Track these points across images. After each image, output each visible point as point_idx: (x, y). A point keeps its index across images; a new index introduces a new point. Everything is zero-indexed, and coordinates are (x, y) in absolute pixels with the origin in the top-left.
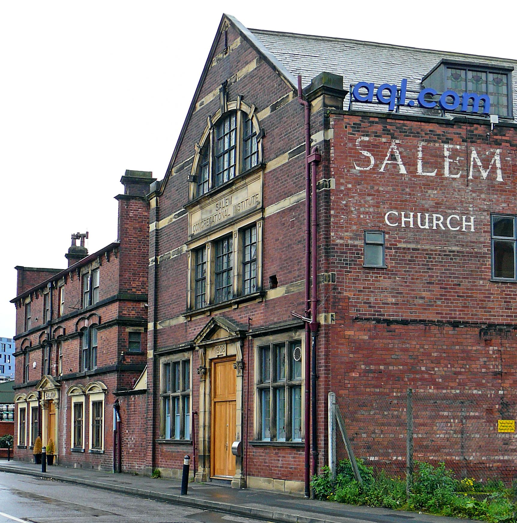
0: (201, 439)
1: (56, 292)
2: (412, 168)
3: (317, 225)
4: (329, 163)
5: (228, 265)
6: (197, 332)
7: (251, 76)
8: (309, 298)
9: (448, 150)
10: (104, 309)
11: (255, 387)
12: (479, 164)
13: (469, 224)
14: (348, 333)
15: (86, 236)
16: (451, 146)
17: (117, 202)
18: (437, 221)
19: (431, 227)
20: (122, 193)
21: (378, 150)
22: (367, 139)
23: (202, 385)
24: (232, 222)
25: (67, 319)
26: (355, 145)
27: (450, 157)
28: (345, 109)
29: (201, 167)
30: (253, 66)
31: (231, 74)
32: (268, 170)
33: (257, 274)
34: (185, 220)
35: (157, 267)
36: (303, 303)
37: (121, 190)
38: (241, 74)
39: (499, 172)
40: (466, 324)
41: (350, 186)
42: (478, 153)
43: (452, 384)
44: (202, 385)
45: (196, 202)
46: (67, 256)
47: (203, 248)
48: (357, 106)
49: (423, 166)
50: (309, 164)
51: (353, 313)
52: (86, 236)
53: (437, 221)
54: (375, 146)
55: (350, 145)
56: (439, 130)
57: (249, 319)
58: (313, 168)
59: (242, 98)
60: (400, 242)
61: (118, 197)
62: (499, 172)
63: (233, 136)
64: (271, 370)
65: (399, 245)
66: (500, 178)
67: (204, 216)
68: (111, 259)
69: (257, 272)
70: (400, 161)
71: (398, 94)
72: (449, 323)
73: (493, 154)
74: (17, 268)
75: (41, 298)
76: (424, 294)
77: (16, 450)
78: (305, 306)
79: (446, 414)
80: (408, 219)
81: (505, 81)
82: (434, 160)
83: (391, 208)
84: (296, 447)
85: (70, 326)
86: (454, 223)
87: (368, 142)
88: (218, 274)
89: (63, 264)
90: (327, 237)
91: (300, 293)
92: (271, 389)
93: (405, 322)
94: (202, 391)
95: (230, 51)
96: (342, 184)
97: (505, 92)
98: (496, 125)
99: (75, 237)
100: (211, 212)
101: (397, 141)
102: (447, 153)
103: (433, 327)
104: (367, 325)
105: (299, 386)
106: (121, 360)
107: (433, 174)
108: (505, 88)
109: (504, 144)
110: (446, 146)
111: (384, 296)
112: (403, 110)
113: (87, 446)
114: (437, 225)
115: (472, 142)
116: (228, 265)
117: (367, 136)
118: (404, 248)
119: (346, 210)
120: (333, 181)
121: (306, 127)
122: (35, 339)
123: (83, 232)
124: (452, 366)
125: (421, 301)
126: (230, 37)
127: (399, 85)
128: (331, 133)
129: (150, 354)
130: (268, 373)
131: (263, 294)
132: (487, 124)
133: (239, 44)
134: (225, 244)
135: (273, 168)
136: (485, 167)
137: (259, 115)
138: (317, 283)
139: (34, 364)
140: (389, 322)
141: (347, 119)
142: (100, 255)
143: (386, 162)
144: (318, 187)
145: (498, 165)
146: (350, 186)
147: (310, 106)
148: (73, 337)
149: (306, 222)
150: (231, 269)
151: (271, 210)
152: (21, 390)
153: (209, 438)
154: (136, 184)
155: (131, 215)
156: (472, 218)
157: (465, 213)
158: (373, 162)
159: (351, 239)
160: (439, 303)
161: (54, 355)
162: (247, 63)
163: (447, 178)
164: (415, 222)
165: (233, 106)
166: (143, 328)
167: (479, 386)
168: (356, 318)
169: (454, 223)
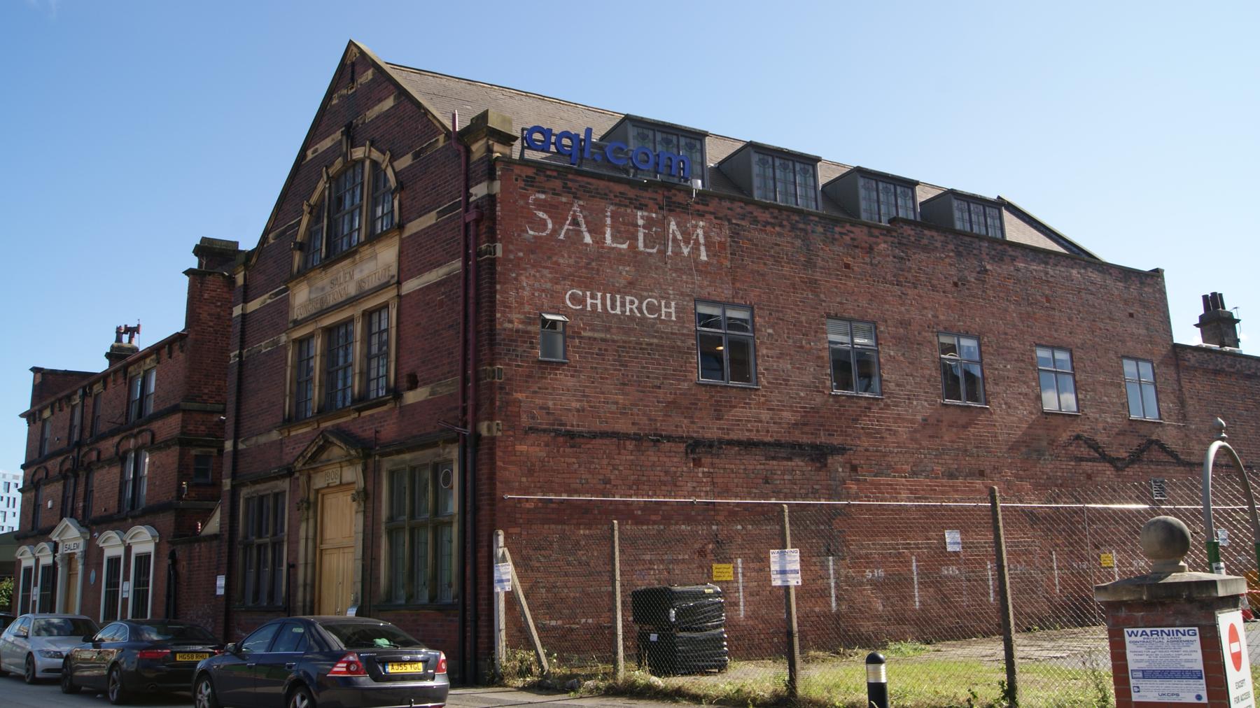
0: (300, 604)
1: (90, 401)
2: (598, 237)
3: (478, 304)
4: (495, 224)
5: (346, 361)
6: (297, 452)
7: (386, 115)
8: (464, 401)
9: (642, 217)
10: (160, 423)
11: (383, 527)
12: (679, 237)
13: (669, 311)
16: (646, 214)
17: (186, 279)
18: (630, 305)
19: (623, 312)
20: (195, 266)
21: (557, 213)
22: (542, 196)
23: (303, 526)
24: (351, 301)
25: (104, 437)
26: (528, 203)
27: (644, 227)
30: (389, 103)
31: (358, 114)
32: (407, 233)
33: (388, 371)
35: (241, 364)
36: (456, 408)
37: (194, 263)
38: (372, 114)
39: (703, 248)
40: (669, 438)
41: (521, 254)
42: (678, 224)
43: (653, 518)
45: (303, 274)
46: (108, 355)
48: (531, 155)
49: (612, 235)
50: (467, 226)
51: (525, 420)
53: (630, 305)
54: (552, 206)
55: (521, 202)
56: (631, 193)
57: (377, 432)
58: (472, 228)
59: (372, 144)
60: (585, 329)
62: (703, 248)
63: (358, 192)
64: (407, 502)
67: (313, 296)
68: (174, 355)
69: (388, 371)
70: (584, 228)
73: (696, 226)
74: (35, 370)
78: (459, 413)
80: (595, 301)
81: (698, 146)
83: (572, 287)
84: (444, 609)
85: (108, 446)
87: (545, 200)
88: (329, 373)
89: (100, 365)
90: (492, 320)
91: (451, 395)
92: (407, 528)
94: (302, 533)
95: (357, 85)
96: (511, 251)
97: (699, 160)
98: (699, 194)
100: (323, 289)
101: (581, 203)
102: (640, 222)
104: (546, 438)
108: (698, 155)
109: (707, 216)
110: (639, 213)
114: (631, 310)
115: (670, 210)
116: (346, 361)
117: (543, 192)
118: (590, 338)
120: (499, 246)
121: (462, 177)
122: (54, 465)
123: (132, 324)
124: (655, 495)
126: (358, 68)
128: (497, 187)
129: (227, 483)
132: (689, 191)
133: (370, 77)
134: (342, 331)
135: (415, 230)
136: (687, 242)
137: (395, 164)
140: (571, 435)
142: (157, 349)
143: (566, 227)
144: (479, 254)
145: (702, 240)
146: (521, 254)
147: (468, 151)
148: (110, 462)
149: (461, 300)
150: (351, 365)
153: (312, 602)
154: (214, 257)
155: (206, 296)
156: (673, 304)
158: (550, 226)
161: (81, 490)
162: (380, 100)
164: (604, 304)
165: (358, 153)
168: (530, 429)
169: (651, 309)
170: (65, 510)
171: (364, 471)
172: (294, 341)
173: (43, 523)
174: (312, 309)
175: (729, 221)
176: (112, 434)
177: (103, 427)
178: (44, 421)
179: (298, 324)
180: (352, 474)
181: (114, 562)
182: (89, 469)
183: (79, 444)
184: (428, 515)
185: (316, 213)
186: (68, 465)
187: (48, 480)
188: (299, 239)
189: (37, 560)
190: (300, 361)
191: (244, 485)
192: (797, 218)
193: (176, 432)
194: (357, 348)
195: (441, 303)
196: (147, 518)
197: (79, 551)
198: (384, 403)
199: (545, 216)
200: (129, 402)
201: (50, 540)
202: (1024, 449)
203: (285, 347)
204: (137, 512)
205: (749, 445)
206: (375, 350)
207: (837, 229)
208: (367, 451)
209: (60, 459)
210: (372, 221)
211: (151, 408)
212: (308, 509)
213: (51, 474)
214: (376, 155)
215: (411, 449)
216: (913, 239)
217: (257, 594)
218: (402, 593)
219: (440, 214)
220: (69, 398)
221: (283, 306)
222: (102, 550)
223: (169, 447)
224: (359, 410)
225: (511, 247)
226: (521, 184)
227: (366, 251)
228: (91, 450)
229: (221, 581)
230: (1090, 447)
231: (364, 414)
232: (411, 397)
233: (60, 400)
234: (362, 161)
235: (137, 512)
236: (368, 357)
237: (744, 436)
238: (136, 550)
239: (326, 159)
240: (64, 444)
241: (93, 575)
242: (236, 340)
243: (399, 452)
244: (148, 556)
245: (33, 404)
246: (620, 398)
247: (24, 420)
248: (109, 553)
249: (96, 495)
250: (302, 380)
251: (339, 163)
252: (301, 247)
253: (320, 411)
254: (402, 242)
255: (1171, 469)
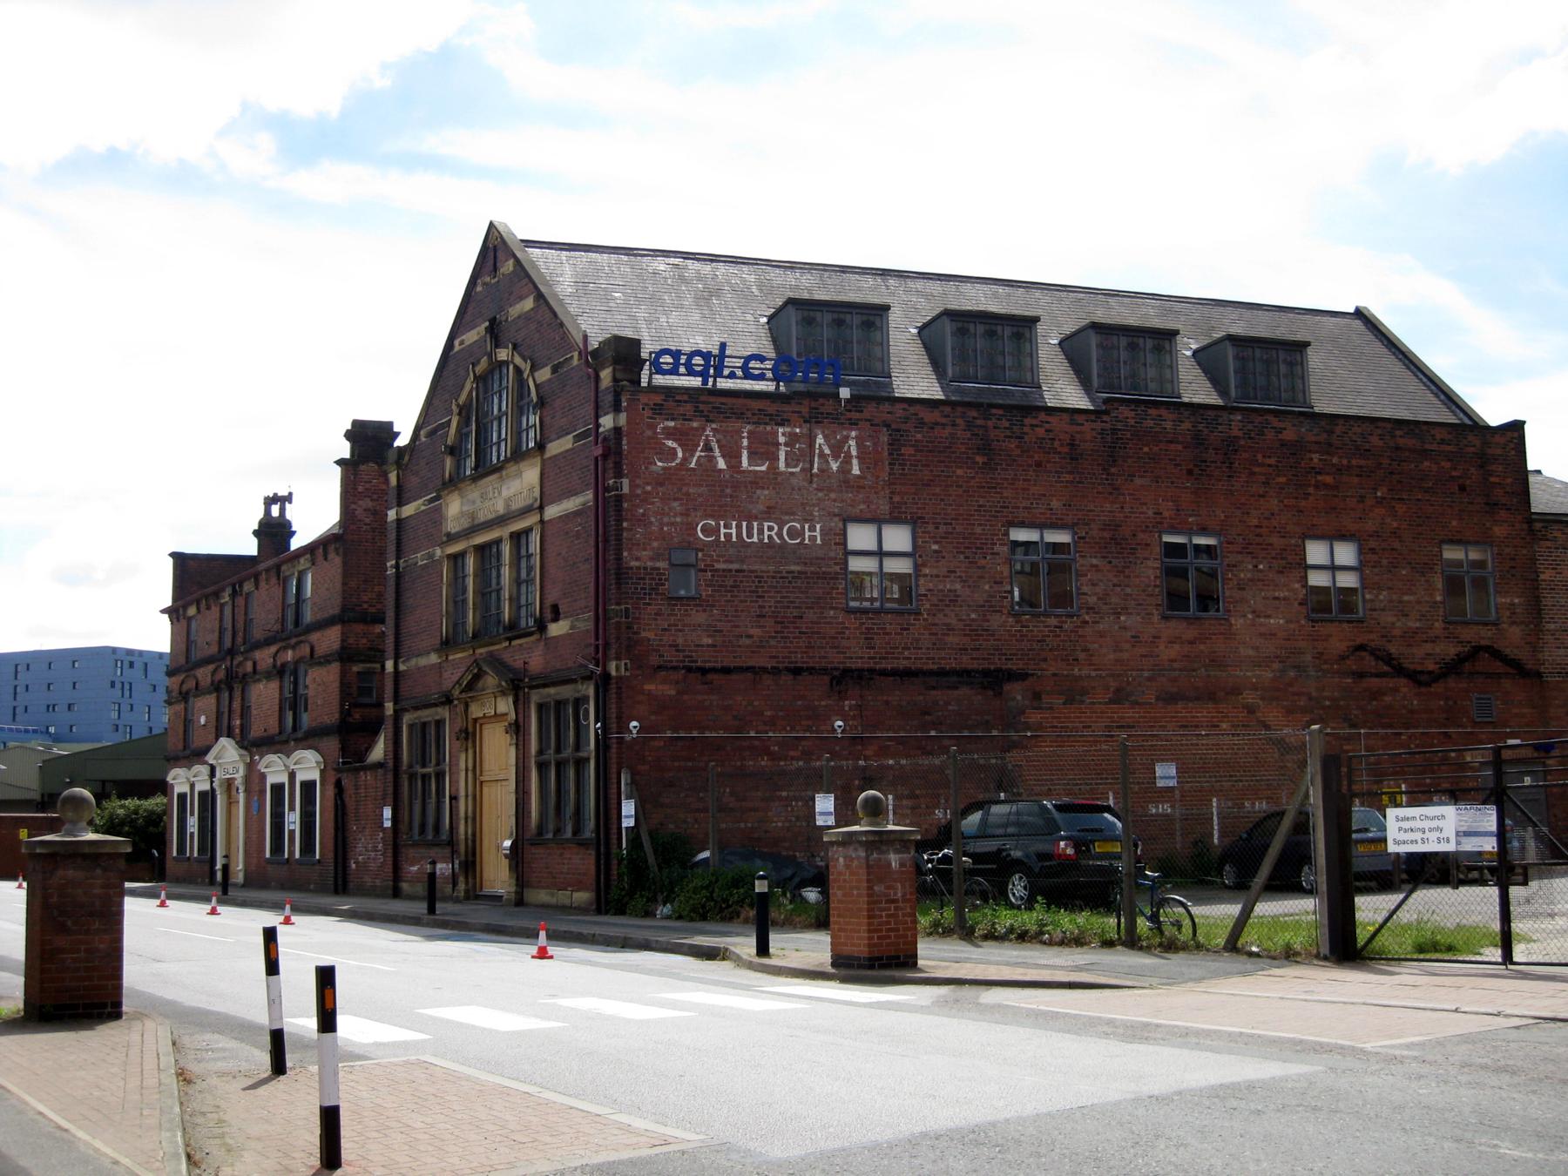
0: (462, 837)
1: (240, 601)
3: (606, 541)
12: (827, 451)
14: (647, 687)
15: (289, 498)
16: (788, 429)
17: (338, 469)
18: (769, 531)
19: (761, 540)
20: (347, 455)
21: (687, 440)
22: (672, 424)
23: (463, 756)
24: (501, 521)
25: (259, 645)
27: (786, 444)
28: (644, 383)
29: (462, 436)
30: (528, 304)
32: (547, 455)
34: (438, 510)
39: (855, 462)
40: (811, 670)
41: (649, 488)
43: (792, 753)
44: (463, 756)
45: (453, 483)
46: (256, 533)
47: (461, 555)
48: (659, 380)
51: (654, 660)
52: (289, 498)
53: (769, 531)
55: (649, 433)
59: (515, 347)
61: (340, 462)
62: (855, 462)
65: (717, 566)
66: (856, 471)
70: (717, 453)
71: (715, 361)
72: (788, 669)
73: (847, 438)
74: (174, 555)
75: (215, 610)
76: (752, 631)
77: (169, 865)
78: (592, 649)
79: (784, 794)
80: (730, 531)
82: (764, 449)
83: (707, 516)
85: (264, 657)
86: (793, 533)
87: (675, 428)
88: (483, 595)
89: (250, 547)
90: (619, 558)
93: (726, 671)
94: (462, 765)
98: (847, 401)
99: (270, 501)
102: (782, 439)
103: (765, 676)
105: (588, 760)
106: (345, 714)
107: (763, 468)
110: (781, 430)
111: (696, 634)
112: (723, 384)
113: (292, 852)
114: (770, 537)
119: (643, 520)
120: (626, 482)
122: (204, 674)
123: (283, 492)
124: (793, 729)
125: (748, 642)
126: (500, 255)
127: (716, 351)
128: (623, 419)
130: (330, 804)
131: (541, 627)
136: (836, 457)
138: (606, 619)
139: (203, 720)
140: (704, 671)
141: (644, 399)
144: (607, 489)
145: (854, 453)
146: (649, 488)
147: (597, 378)
148: (268, 676)
151: (552, 512)
152: (390, 853)
153: (474, 834)
154: (369, 440)
155: (360, 489)
157: (810, 520)
158: (680, 454)
159: (652, 559)
160: (773, 642)
161: (236, 705)
162: (521, 298)
163: (781, 473)
164: (739, 534)
165: (503, 355)
166: (378, 666)
167: (834, 755)
168: (659, 667)
169: (793, 533)
170: (222, 728)
171: (516, 703)
172: (449, 556)
173: (197, 741)
174: (465, 523)
175: (888, 426)
176: (268, 642)
177: (257, 634)
178: (189, 619)
179: (452, 538)
180: (505, 705)
181: (278, 789)
182: (245, 680)
183: (232, 652)
184: (570, 750)
185: (464, 411)
186: (221, 675)
187: (199, 690)
188: (449, 442)
189: (192, 786)
190: (456, 579)
191: (406, 710)
192: (975, 414)
193: (336, 646)
194: (506, 572)
195: (578, 535)
196: (310, 741)
197: (239, 776)
198: (531, 634)
199: (675, 445)
200: (284, 606)
201: (206, 763)
202: (1276, 666)
203: (440, 562)
204: (300, 735)
205: (907, 674)
206: (524, 575)
207: (1027, 421)
208: (517, 685)
209: (211, 667)
210: (518, 433)
211: (308, 616)
212: (466, 739)
213: (202, 683)
214: (518, 360)
215: (554, 684)
216: (1132, 422)
217: (423, 826)
218: (551, 826)
219: (577, 438)
220: (217, 595)
221: (435, 515)
222: (263, 777)
223: (329, 662)
224: (510, 639)
225: (638, 481)
226: (648, 413)
227: (512, 469)
228: (246, 659)
229: (387, 813)
230: (1377, 658)
231: (515, 643)
232: (556, 629)
233: (207, 597)
234: (506, 363)
235: (300, 735)
236: (518, 582)
237: (902, 664)
238: (300, 777)
239: (471, 355)
240: (214, 649)
241: (255, 805)
242: (392, 548)
243: (545, 686)
244: (314, 782)
245: (175, 599)
246: (755, 632)
247: (166, 616)
248: (271, 780)
249: (254, 712)
250: (458, 603)
251: (483, 364)
252: (452, 451)
253: (475, 636)
254: (543, 463)
255: (1507, 684)
